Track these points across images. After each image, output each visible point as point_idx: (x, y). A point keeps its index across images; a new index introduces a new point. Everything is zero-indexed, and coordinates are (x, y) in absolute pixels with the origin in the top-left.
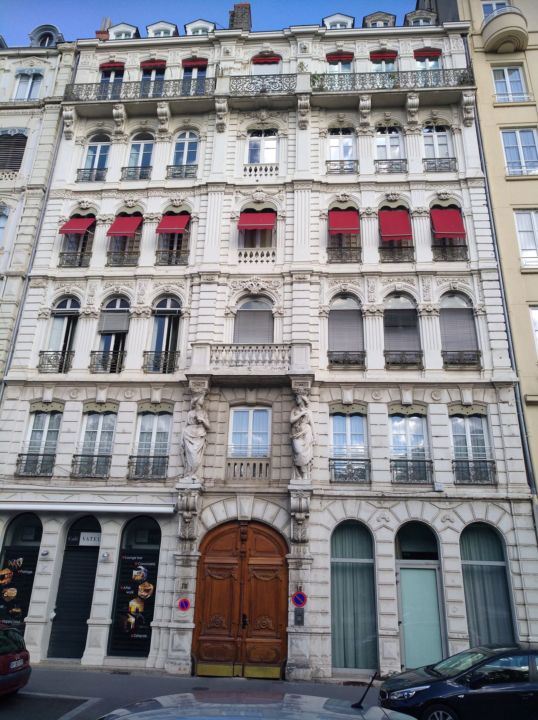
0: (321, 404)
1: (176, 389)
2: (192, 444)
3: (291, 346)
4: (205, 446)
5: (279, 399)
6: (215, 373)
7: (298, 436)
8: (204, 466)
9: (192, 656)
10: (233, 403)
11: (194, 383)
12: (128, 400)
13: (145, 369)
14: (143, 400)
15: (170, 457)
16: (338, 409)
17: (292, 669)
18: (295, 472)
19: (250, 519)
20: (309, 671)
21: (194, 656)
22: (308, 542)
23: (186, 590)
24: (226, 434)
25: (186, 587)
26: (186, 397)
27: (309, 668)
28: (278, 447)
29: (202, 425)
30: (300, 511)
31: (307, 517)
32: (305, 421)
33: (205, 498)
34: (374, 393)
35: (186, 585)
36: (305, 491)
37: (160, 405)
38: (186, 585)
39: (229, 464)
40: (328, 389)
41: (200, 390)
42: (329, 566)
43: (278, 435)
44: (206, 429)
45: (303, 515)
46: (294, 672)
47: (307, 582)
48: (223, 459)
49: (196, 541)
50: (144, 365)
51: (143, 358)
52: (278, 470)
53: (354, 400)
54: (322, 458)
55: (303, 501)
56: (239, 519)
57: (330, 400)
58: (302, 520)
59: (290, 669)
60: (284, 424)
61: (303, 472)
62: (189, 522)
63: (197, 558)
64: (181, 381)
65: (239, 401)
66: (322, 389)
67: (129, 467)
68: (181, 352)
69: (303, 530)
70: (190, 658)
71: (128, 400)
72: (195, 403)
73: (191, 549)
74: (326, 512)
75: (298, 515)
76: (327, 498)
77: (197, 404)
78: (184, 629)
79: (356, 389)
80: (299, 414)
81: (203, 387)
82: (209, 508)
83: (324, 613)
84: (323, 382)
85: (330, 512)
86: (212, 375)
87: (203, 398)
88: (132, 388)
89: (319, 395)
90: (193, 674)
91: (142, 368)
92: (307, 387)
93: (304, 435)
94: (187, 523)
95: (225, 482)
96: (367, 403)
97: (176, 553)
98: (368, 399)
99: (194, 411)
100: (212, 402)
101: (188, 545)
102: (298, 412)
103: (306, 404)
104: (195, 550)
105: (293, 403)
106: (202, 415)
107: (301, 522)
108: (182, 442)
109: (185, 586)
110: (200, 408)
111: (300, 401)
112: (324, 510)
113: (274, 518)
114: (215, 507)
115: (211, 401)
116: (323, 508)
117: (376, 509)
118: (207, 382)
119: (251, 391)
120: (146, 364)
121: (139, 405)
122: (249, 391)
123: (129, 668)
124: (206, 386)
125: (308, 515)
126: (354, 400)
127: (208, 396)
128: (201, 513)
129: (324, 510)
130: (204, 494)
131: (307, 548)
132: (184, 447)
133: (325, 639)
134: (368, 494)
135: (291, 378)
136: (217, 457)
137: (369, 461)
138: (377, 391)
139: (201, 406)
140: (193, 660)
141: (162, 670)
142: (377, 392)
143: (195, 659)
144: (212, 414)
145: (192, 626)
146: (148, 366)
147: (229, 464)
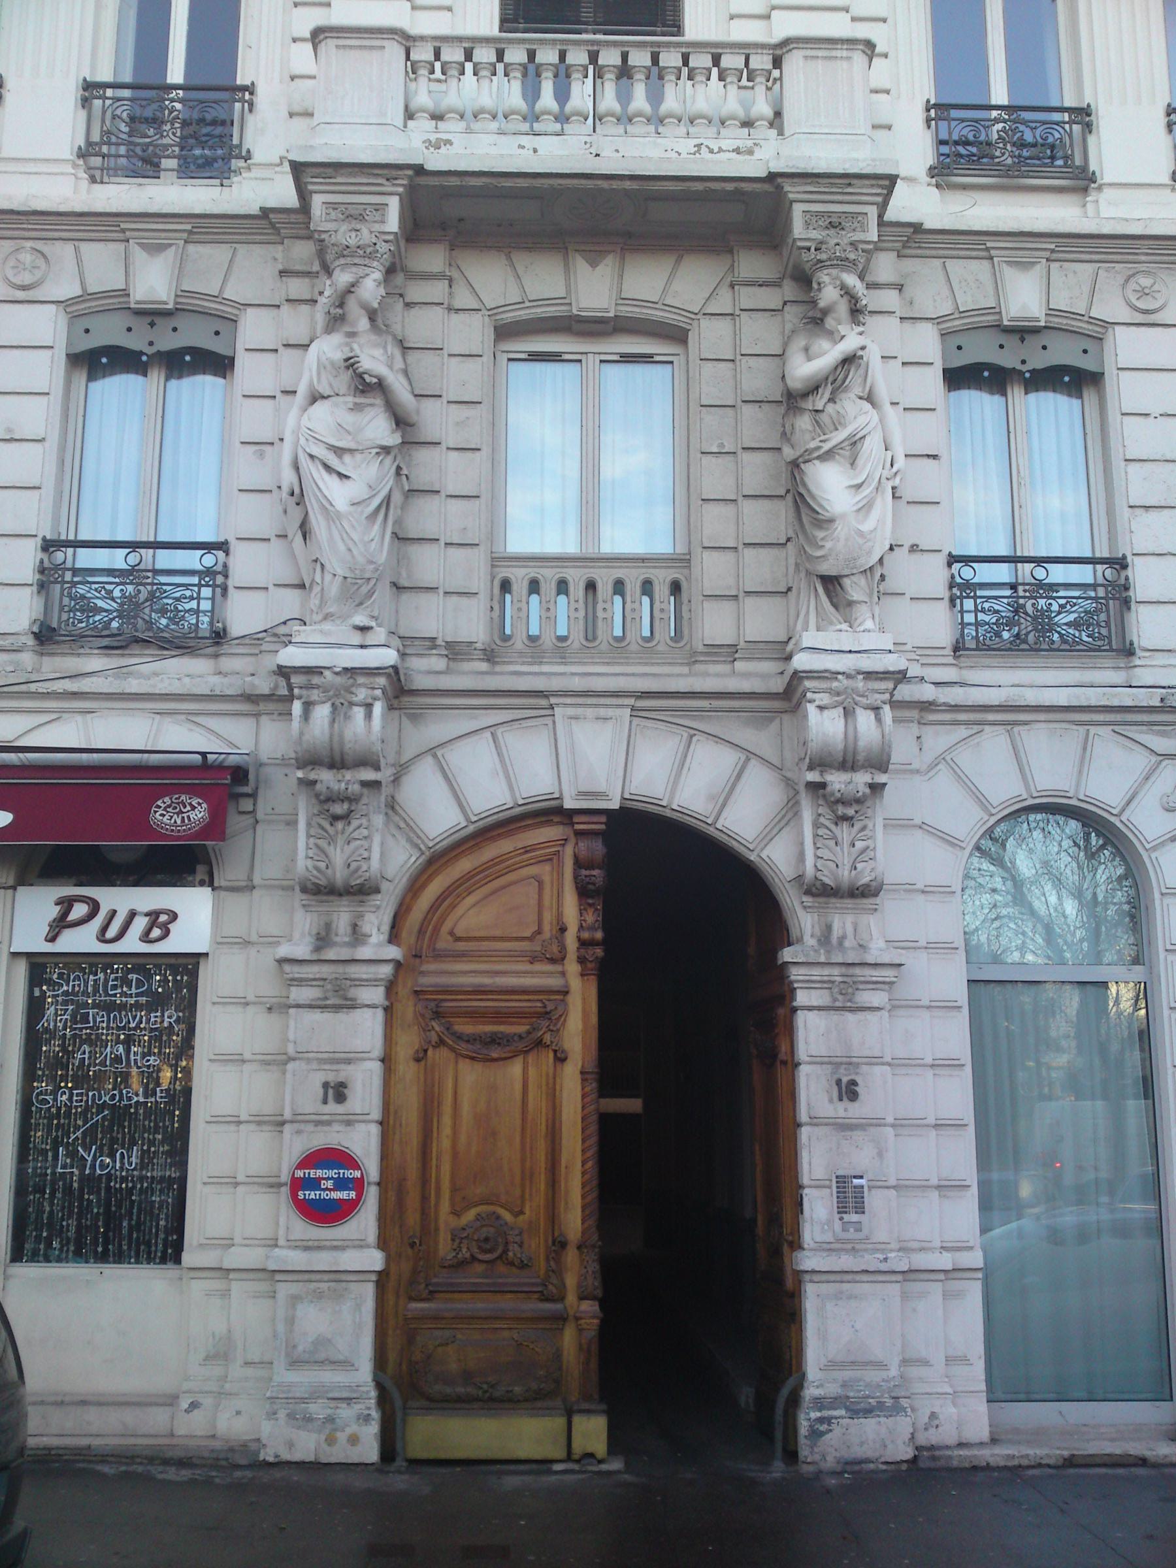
0: (907, 325)
1: (242, 249)
2: (342, 476)
3: (779, 53)
4: (397, 498)
5: (723, 302)
6: (436, 161)
7: (826, 447)
8: (397, 587)
9: (380, 1386)
10: (509, 317)
11: (333, 206)
12: (21, 295)
13: (96, 161)
14: (95, 296)
15: (235, 546)
16: (982, 350)
17: (828, 1420)
18: (813, 602)
19: (615, 805)
20: (902, 1426)
21: (389, 1384)
22: (876, 894)
23: (339, 1109)
24: (486, 450)
25: (341, 1098)
26: (298, 287)
27: (896, 1409)
28: (728, 510)
29: (379, 401)
30: (848, 763)
31: (876, 788)
32: (855, 386)
33: (414, 718)
34: (1132, 285)
35: (342, 1085)
36: (869, 675)
37: (174, 322)
38: (342, 1085)
39: (506, 586)
40: (937, 263)
41: (366, 237)
42: (961, 994)
43: (721, 460)
44: (401, 421)
45: (861, 779)
46: (837, 1431)
47: (875, 1060)
48: (478, 560)
49: (376, 900)
50: (89, 144)
51: (82, 114)
52: (729, 606)
53: (1051, 312)
54: (916, 556)
55: (865, 721)
56: (569, 804)
57: (946, 308)
58: (858, 801)
59: (821, 1420)
60: (748, 410)
61: (850, 604)
62: (346, 817)
63: (386, 970)
64: (265, 212)
65: (542, 312)
66: (909, 265)
67: (42, 587)
68: (260, 90)
69: (859, 845)
70: (373, 1394)
71: (21, 295)
72: (343, 298)
73: (357, 936)
74: (943, 776)
75: (837, 781)
76: (948, 717)
77: (352, 304)
78: (337, 1275)
79: (1054, 266)
80: (828, 355)
81: (377, 227)
82: (429, 760)
83: (947, 1188)
84: (917, 228)
85: (962, 779)
86: (419, 170)
87: (378, 275)
88: (39, 245)
89: (900, 288)
90: (388, 1452)
91: (82, 154)
92: (858, 236)
93: (855, 442)
94: (336, 818)
95: (490, 656)
96: (1106, 325)
97: (284, 951)
98: (1110, 307)
99: (337, 338)
100: (415, 311)
101: (342, 917)
102: (825, 344)
103: (856, 312)
104: (374, 940)
105: (792, 315)
106: (378, 353)
107: (850, 812)
108: (288, 478)
109: (338, 1091)
110: (363, 323)
111: (829, 295)
112: (933, 766)
113: (725, 799)
114: (456, 757)
115: (408, 305)
116: (929, 757)
117: (1154, 759)
118: (394, 203)
119: (593, 264)
120: (96, 137)
121: (74, 318)
122: (581, 265)
123: (96, 1442)
124: (393, 223)
125: (881, 778)
126: (1051, 312)
127: (399, 279)
128: (396, 780)
129: (933, 766)
130: (406, 700)
131: (872, 921)
132: (298, 496)
133: (959, 1295)
134: (1126, 697)
135: (792, 190)
136: (452, 551)
137: (1120, 564)
138: (1147, 273)
139: (372, 316)
140: (384, 1400)
141: (242, 1448)
142: (1145, 281)
143: (396, 1395)
144: (423, 364)
145: (375, 1260)
146: (105, 149)
147: (506, 586)
